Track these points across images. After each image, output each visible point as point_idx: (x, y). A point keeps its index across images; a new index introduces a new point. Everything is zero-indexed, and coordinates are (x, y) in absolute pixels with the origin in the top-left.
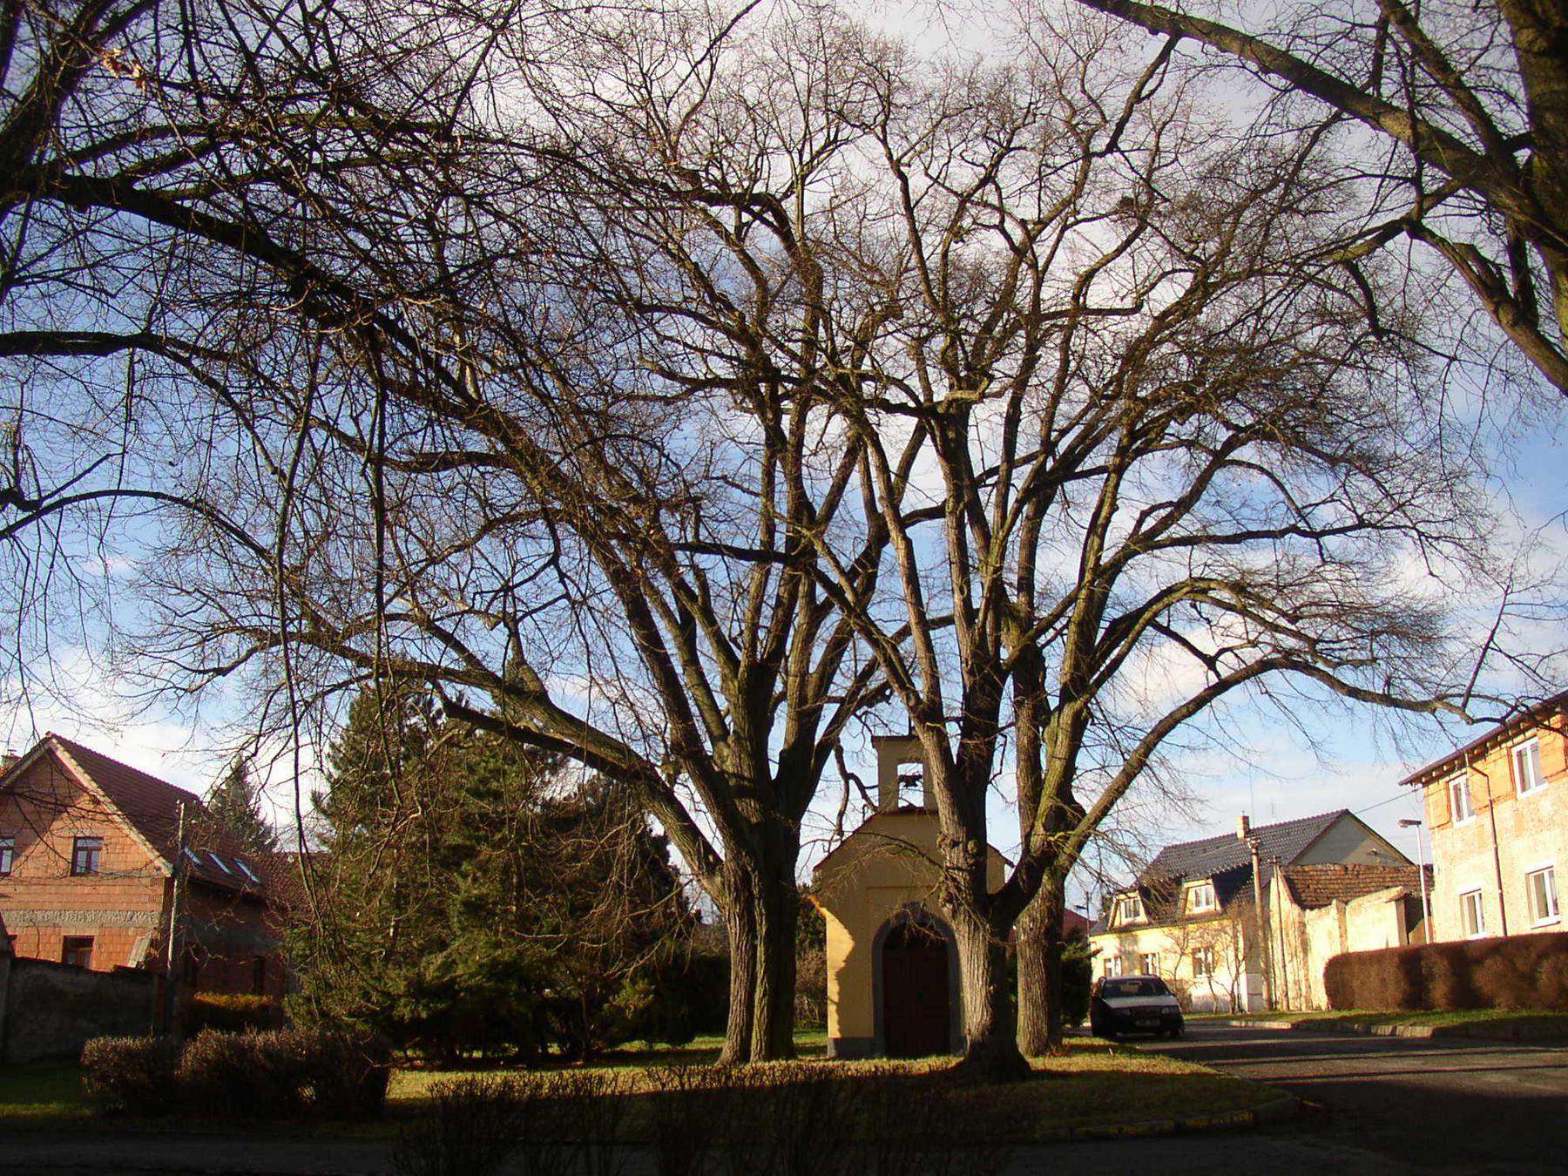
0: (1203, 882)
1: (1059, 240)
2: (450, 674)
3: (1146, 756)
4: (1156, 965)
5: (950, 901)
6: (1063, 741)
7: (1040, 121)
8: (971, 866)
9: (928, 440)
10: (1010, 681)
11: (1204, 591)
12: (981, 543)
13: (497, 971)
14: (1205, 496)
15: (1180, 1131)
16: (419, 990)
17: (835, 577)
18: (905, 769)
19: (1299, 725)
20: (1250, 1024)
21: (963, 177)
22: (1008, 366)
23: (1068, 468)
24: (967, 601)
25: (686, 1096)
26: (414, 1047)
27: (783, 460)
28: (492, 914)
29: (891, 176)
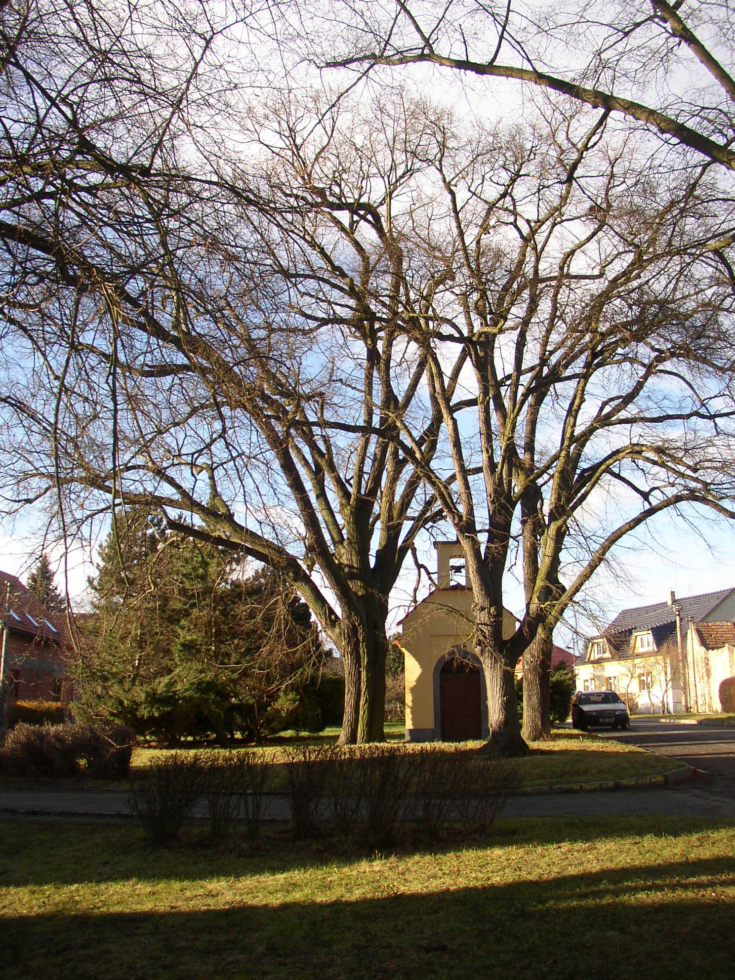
0: (645, 632)
1: (550, 232)
2: (171, 503)
3: (604, 554)
5: (479, 644)
6: (551, 544)
7: (539, 158)
9: (468, 359)
10: (518, 507)
11: (640, 453)
12: (501, 421)
13: (204, 688)
14: (641, 393)
15: (618, 788)
16: (153, 699)
17: (408, 443)
18: (455, 562)
19: (701, 535)
21: (492, 192)
22: (518, 311)
23: (555, 376)
24: (491, 458)
25: (307, 764)
26: (152, 734)
27: (379, 369)
28: (199, 651)
29: (446, 193)
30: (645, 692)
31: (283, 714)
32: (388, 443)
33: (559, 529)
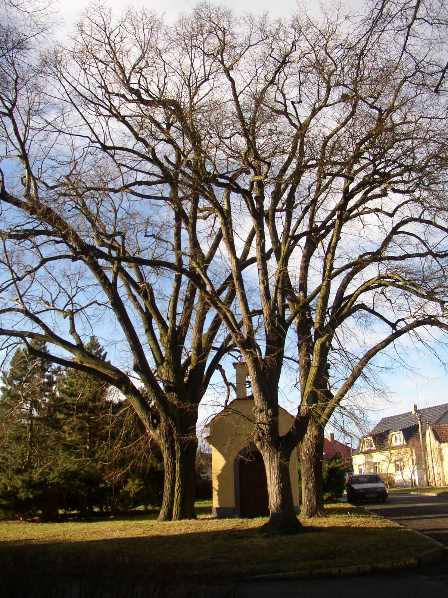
0: (398, 432)
4: (380, 467)
5: (259, 440)
8: (270, 422)
16: (29, 485)
20: (419, 493)
30: (399, 472)
31: (131, 495)
32: (181, 275)
33: (323, 345)
